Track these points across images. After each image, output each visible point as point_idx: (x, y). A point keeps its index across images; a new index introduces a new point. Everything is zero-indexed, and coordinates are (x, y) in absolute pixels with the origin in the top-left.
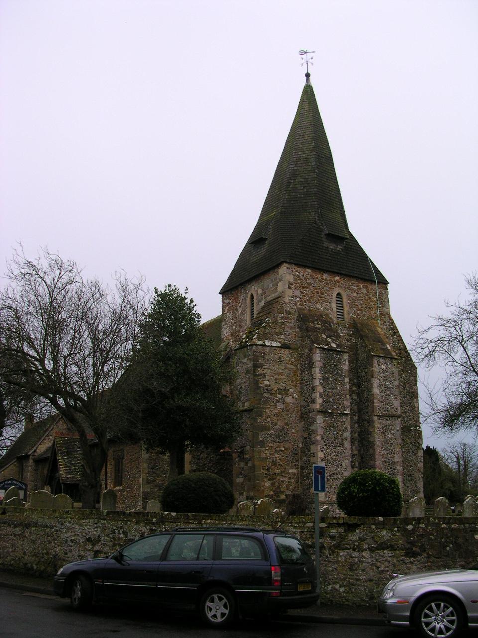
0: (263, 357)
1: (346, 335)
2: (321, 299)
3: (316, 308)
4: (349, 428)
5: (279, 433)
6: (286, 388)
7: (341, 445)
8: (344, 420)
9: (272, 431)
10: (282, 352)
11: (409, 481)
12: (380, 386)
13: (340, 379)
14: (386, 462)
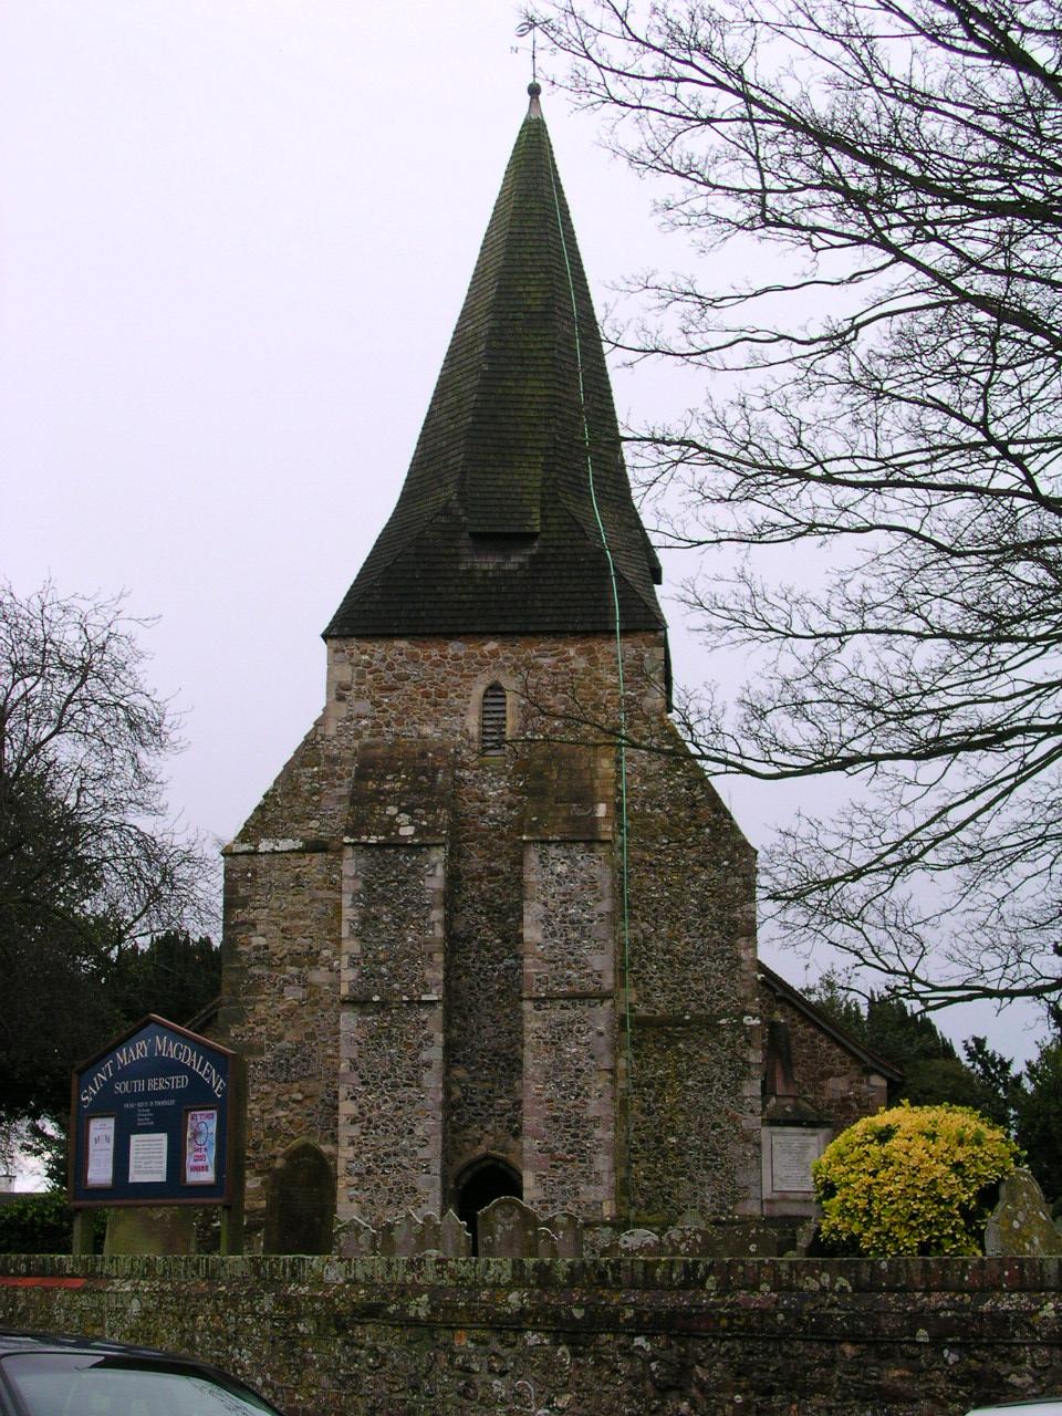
0: (249, 880)
1: (506, 791)
2: (435, 711)
3: (419, 736)
4: (439, 1037)
5: (288, 1060)
6: (311, 948)
7: (414, 1080)
8: (424, 1017)
9: (268, 1056)
10: (306, 862)
11: (708, 1168)
12: (547, 920)
13: (415, 915)
14: (556, 1119)
